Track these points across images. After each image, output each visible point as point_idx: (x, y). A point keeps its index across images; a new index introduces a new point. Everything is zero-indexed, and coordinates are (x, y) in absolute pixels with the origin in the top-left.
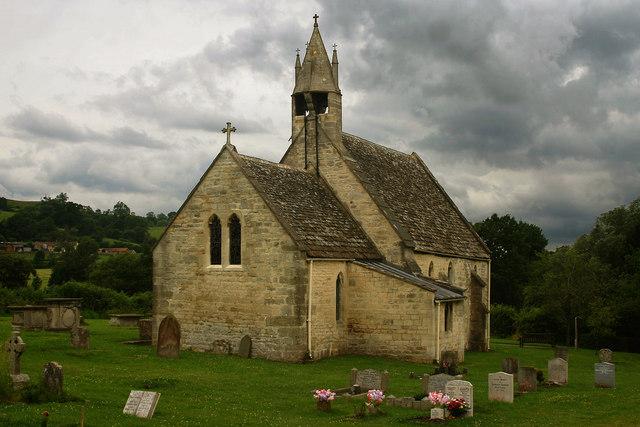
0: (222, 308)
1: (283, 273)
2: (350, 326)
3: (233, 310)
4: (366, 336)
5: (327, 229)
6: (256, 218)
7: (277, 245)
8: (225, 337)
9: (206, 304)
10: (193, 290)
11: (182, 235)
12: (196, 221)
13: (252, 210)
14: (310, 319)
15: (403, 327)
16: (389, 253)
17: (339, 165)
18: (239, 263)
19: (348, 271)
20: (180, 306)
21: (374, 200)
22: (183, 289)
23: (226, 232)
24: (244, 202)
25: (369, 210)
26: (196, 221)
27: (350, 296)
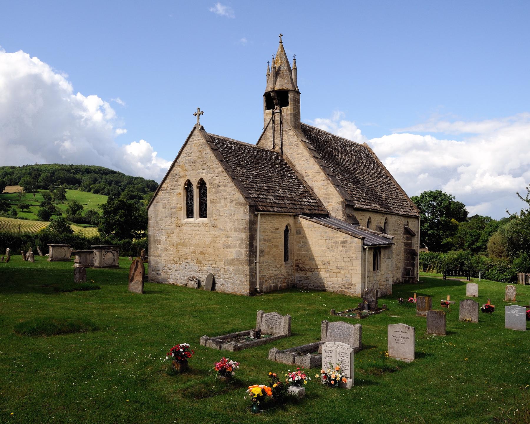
0: (194, 252)
1: (236, 224)
2: (297, 266)
3: (202, 253)
4: (309, 274)
5: (281, 191)
7: (231, 202)
8: (196, 275)
9: (183, 249)
10: (175, 239)
11: (168, 196)
12: (176, 185)
13: (215, 174)
14: (257, 261)
15: (337, 267)
16: (333, 210)
17: (297, 145)
18: (206, 217)
19: (295, 223)
20: (166, 250)
21: (324, 170)
22: (168, 237)
23: (196, 192)
24: (208, 168)
25: (217, 163)
26: (176, 185)
27: (299, 242)
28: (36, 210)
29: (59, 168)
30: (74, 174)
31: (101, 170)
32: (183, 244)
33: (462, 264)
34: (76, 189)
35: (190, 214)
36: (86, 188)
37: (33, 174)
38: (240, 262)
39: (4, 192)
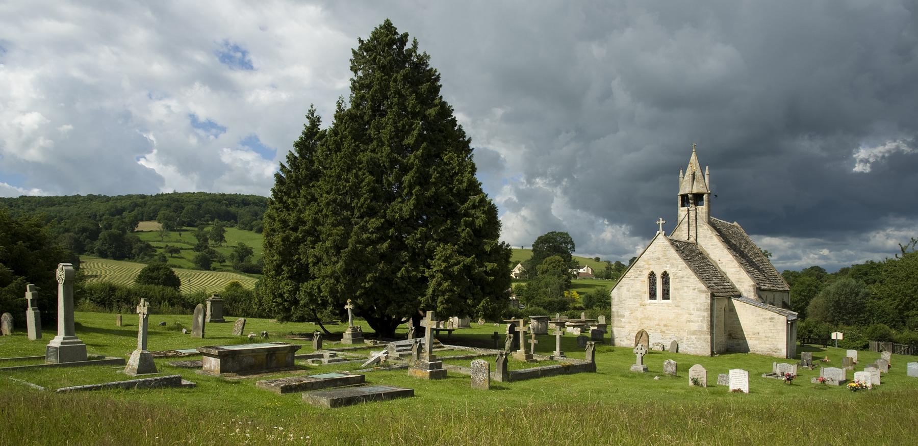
0: (658, 325)
2: (730, 335)
3: (665, 326)
6: (680, 274)
8: (659, 341)
10: (639, 314)
28: (192, 255)
29: (207, 198)
30: (227, 205)
31: (262, 201)
32: (647, 318)
33: (811, 332)
34: (232, 226)
35: (653, 296)
36: (246, 225)
37: (173, 205)
38: (702, 333)
39: (136, 230)
